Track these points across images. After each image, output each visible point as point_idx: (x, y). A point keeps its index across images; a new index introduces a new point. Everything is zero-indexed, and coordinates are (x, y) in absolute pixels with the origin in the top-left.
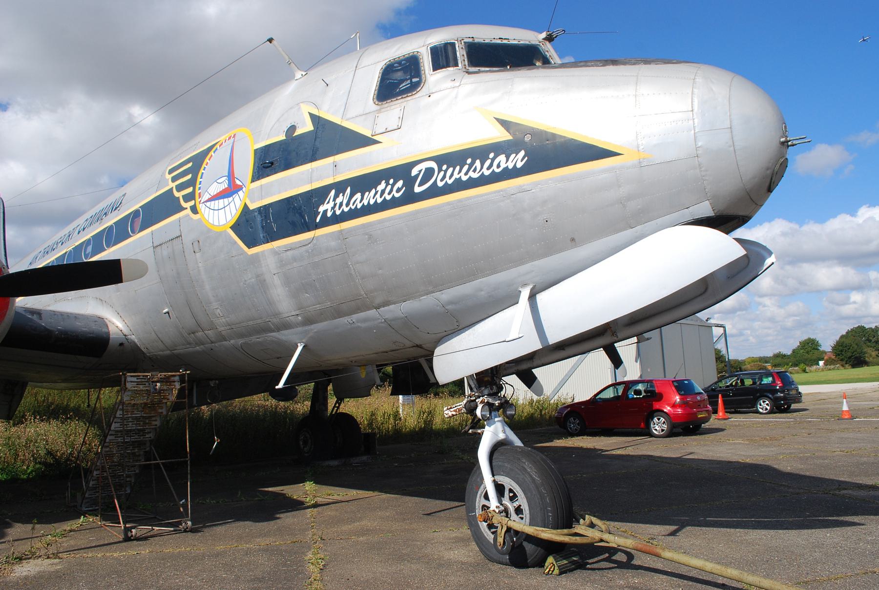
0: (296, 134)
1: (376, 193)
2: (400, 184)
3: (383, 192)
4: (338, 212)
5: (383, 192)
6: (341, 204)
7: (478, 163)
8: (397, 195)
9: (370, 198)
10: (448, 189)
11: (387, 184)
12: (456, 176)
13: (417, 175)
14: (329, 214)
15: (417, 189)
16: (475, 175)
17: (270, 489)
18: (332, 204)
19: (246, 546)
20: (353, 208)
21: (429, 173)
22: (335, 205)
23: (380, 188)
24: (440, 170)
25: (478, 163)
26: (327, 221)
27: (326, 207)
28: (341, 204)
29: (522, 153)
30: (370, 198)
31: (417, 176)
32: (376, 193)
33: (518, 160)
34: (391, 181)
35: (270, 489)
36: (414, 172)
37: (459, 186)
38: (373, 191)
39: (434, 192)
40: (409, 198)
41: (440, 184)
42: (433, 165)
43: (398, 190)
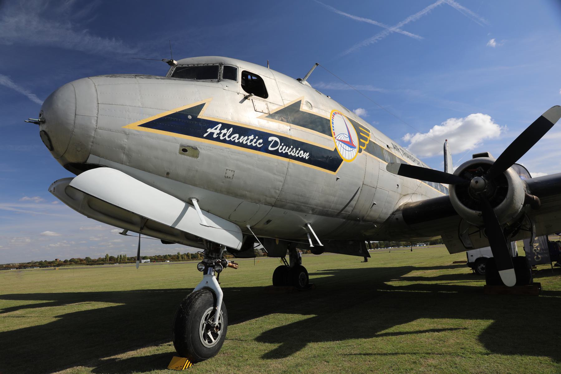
0: (490, 322)
1: (248, 139)
2: (261, 141)
3: (251, 141)
4: (222, 138)
5: (251, 141)
6: (225, 135)
7: (294, 150)
8: (259, 146)
9: (243, 140)
10: (282, 155)
11: (255, 138)
12: (286, 151)
13: (271, 142)
14: (215, 136)
15: (270, 148)
16: (293, 154)
17: (120, 304)
18: (218, 131)
19: (471, 356)
20: (233, 140)
21: (276, 144)
22: (220, 133)
23: (251, 137)
24: (281, 145)
25: (294, 150)
26: (210, 137)
27: (215, 131)
28: (225, 135)
29: (308, 154)
30: (243, 140)
31: (271, 142)
32: (248, 139)
33: (306, 156)
34: (257, 137)
35: (120, 304)
36: (270, 139)
37: (286, 155)
38: (246, 138)
39: (276, 153)
40: (264, 149)
41: (280, 151)
42: (278, 140)
43: (260, 144)
